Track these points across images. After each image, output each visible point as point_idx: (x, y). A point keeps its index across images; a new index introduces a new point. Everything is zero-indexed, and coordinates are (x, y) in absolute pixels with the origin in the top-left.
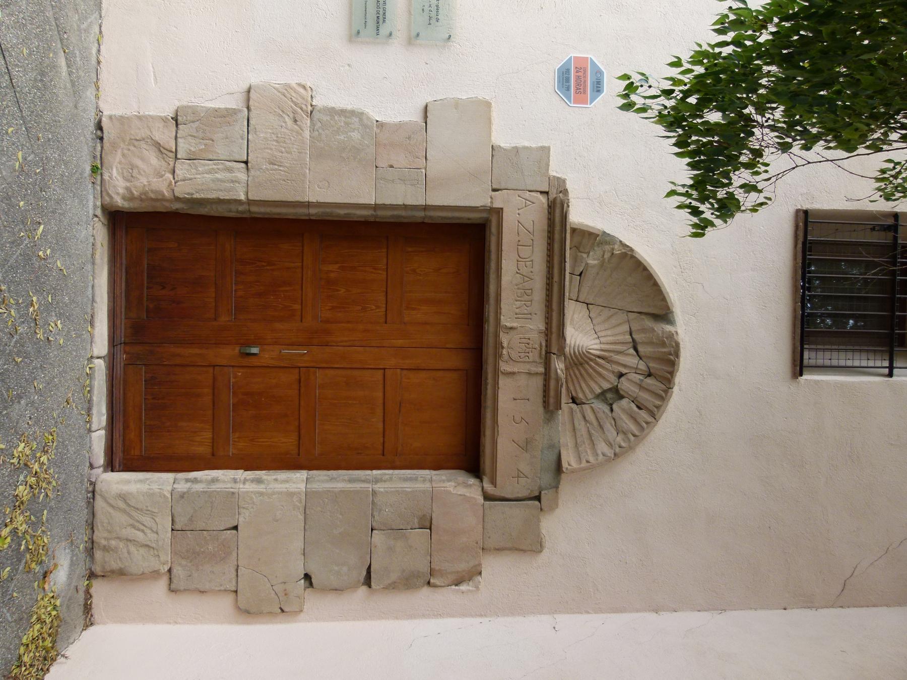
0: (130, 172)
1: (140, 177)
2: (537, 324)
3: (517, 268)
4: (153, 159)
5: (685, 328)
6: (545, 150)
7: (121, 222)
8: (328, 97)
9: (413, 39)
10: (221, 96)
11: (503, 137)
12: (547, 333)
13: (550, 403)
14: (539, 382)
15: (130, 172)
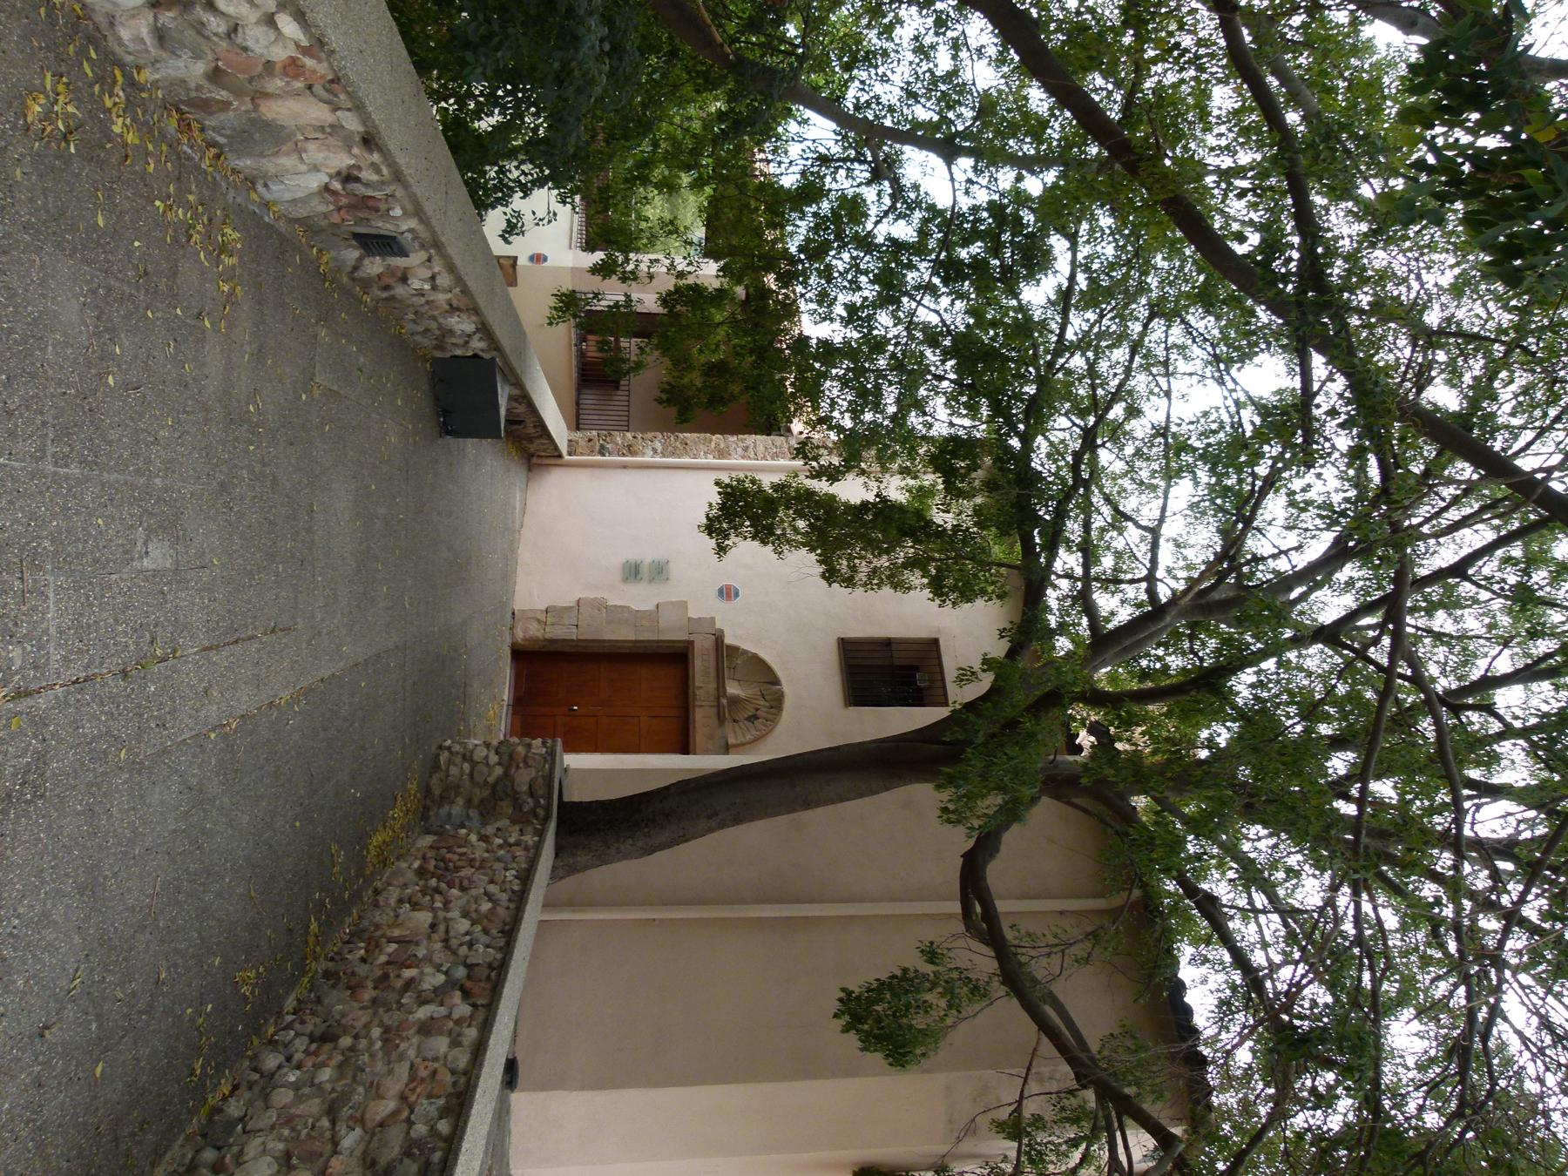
0: (525, 630)
1: (528, 631)
2: (712, 686)
3: (701, 666)
4: (535, 625)
5: (786, 687)
6: (713, 619)
7: (525, 656)
8: (614, 600)
9: (651, 581)
10: (567, 600)
11: (693, 614)
12: (718, 689)
13: (721, 720)
14: (714, 710)
15: (525, 630)
